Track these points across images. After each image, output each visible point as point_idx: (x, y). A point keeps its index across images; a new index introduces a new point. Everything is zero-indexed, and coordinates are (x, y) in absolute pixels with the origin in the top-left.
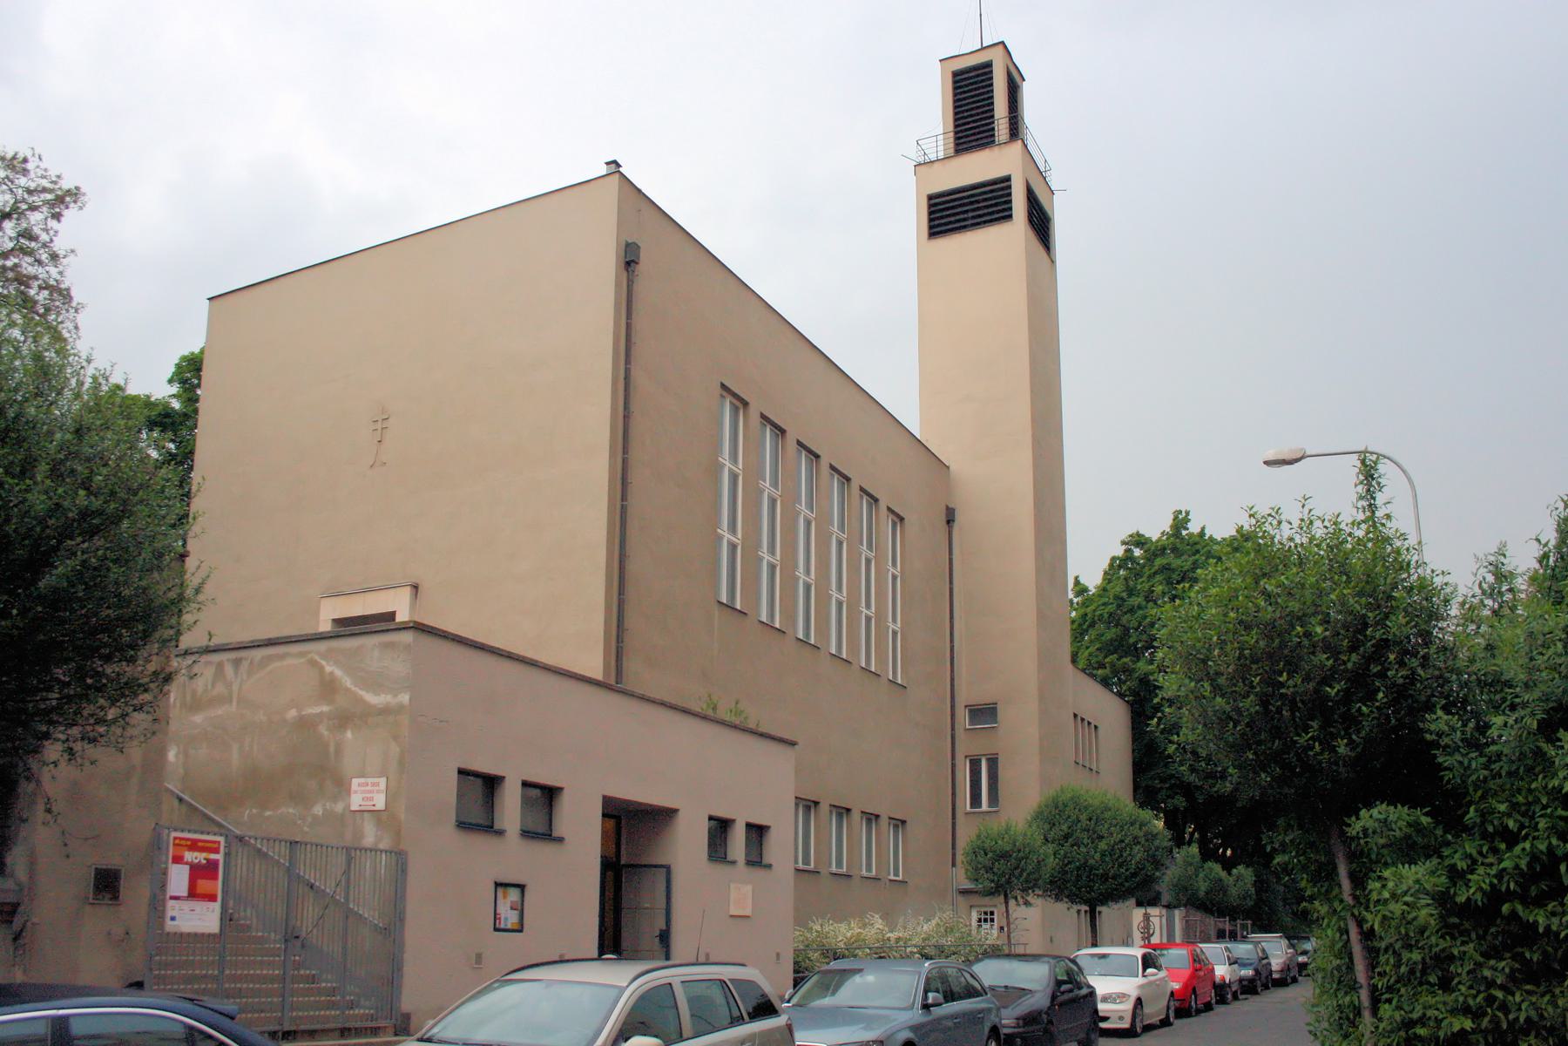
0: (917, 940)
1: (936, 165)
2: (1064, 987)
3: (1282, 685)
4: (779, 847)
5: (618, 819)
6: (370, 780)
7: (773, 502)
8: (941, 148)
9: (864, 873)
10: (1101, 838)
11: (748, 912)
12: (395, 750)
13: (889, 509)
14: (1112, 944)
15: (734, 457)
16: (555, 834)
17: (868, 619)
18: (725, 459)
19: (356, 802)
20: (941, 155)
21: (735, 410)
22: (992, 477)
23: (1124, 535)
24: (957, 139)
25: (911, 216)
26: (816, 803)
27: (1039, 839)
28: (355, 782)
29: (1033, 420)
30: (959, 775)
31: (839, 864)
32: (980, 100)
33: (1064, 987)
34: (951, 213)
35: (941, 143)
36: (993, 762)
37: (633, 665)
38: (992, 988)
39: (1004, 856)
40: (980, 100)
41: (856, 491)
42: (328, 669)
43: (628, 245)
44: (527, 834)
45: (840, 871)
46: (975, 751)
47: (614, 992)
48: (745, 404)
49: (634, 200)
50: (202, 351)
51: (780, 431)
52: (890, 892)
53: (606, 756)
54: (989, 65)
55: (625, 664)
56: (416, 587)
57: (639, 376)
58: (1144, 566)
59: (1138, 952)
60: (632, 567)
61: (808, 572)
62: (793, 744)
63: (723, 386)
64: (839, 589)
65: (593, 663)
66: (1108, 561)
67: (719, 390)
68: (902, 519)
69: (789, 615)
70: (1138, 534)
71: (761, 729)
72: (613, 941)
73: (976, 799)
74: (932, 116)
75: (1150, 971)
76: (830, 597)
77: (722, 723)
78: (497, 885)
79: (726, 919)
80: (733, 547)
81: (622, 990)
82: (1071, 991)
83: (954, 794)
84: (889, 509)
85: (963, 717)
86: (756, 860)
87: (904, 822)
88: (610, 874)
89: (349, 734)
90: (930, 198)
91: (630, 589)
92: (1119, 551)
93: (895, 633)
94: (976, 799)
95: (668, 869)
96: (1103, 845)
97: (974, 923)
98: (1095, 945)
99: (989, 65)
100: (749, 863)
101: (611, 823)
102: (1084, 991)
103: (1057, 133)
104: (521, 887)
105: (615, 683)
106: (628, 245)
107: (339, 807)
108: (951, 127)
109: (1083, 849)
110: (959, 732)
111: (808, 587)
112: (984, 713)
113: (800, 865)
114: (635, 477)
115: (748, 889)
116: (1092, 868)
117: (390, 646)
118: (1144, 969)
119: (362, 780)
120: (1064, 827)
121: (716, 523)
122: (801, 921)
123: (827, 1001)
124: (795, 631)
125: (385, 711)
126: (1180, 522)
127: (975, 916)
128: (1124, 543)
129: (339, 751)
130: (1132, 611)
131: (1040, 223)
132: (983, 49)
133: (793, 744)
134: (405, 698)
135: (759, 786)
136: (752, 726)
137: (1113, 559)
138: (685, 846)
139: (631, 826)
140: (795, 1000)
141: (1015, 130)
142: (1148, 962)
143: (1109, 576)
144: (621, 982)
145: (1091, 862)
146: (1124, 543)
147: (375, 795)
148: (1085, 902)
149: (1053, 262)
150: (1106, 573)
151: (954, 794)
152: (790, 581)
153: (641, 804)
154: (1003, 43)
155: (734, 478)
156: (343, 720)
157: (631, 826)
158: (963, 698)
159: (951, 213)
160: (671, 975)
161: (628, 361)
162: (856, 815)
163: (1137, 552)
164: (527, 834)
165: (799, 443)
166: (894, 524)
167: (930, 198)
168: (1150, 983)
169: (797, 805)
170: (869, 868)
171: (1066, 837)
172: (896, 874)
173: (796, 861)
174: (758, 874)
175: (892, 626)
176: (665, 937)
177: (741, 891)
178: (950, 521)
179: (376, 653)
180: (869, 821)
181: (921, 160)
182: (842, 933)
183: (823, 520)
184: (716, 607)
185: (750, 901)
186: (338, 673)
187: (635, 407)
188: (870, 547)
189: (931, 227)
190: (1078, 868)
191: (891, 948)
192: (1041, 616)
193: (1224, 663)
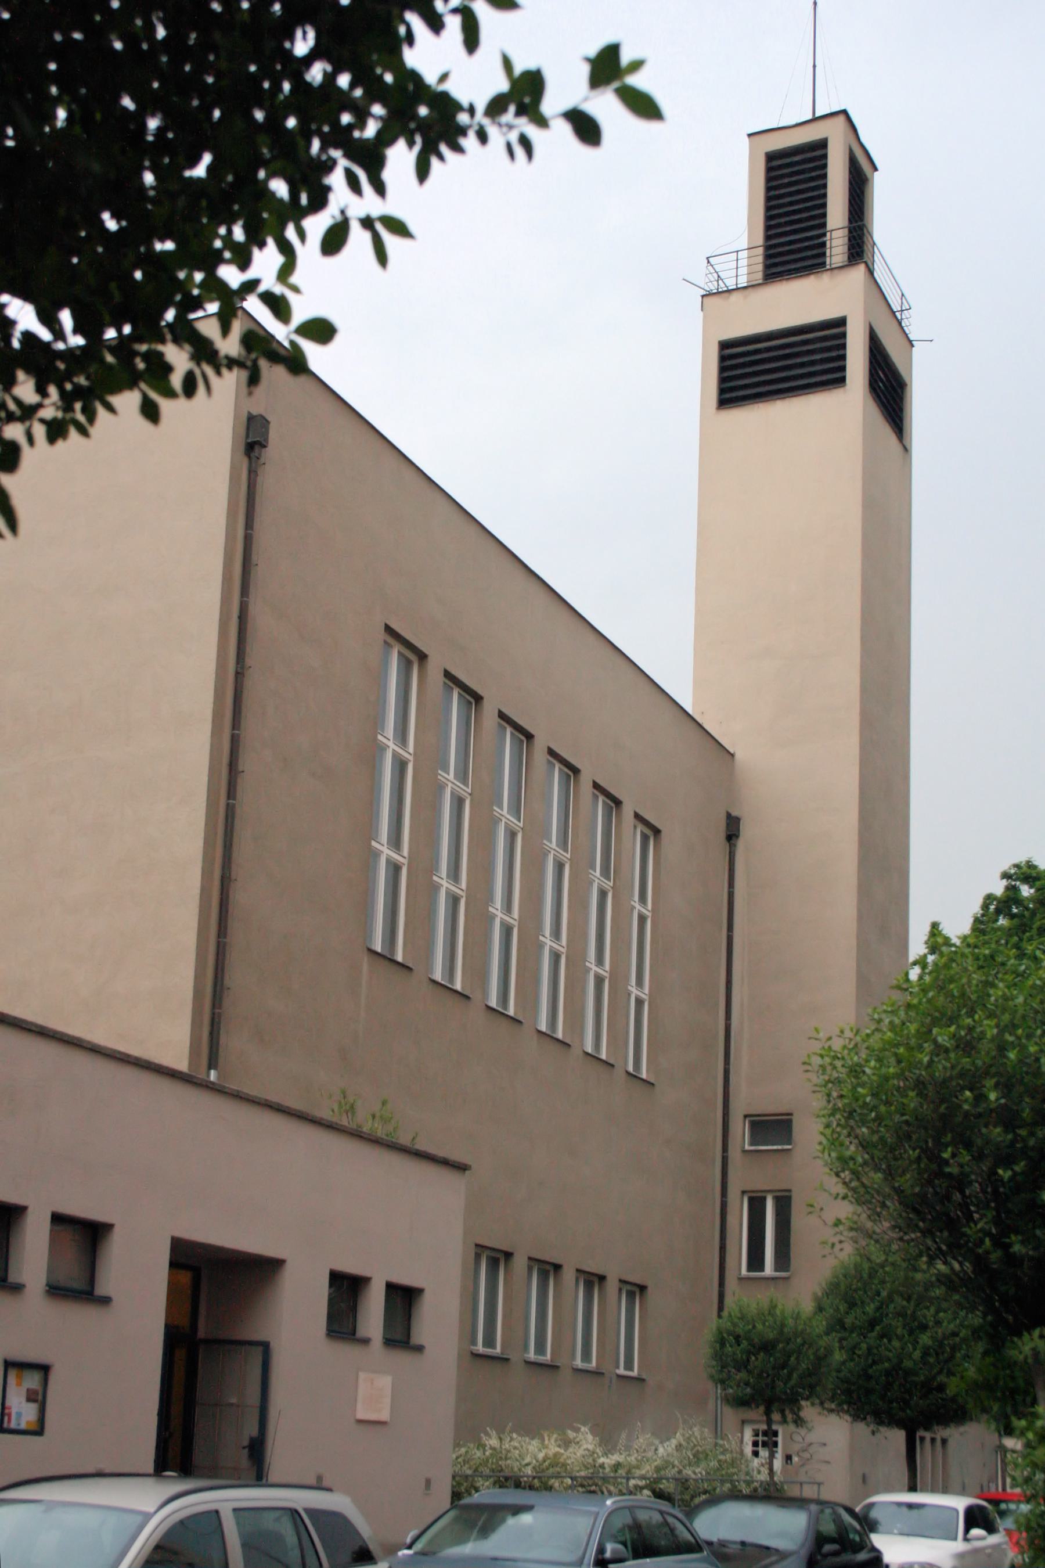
0: (647, 1469)
1: (735, 297)
2: (828, 1548)
3: (946, 1162)
4: (438, 1321)
5: (196, 1272)
7: (459, 802)
8: (743, 271)
9: (579, 1363)
10: (924, 1328)
11: (384, 1415)
13: (637, 816)
14: (933, 1490)
15: (402, 736)
16: (100, 1290)
17: (599, 981)
20: (743, 281)
21: (406, 665)
22: (797, 772)
23: (1006, 864)
24: (767, 257)
25: (695, 373)
26: (508, 1255)
27: (820, 1325)
29: (864, 690)
30: (731, 1220)
31: (540, 1348)
33: (828, 1548)
34: (755, 371)
35: (743, 263)
36: (784, 1204)
37: (236, 1042)
38: (710, 1544)
39: (767, 1347)
41: (586, 787)
43: (251, 419)
44: (56, 1291)
45: (541, 1359)
46: (759, 1182)
47: (139, 1519)
48: (422, 657)
52: (615, 1396)
53: (178, 1180)
54: (822, 145)
55: (223, 1039)
57: (258, 609)
58: (1034, 913)
59: (960, 1503)
60: (240, 897)
61: (508, 908)
62: (462, 1168)
63: (388, 629)
64: (556, 934)
65: (172, 1042)
66: (979, 901)
67: (381, 635)
68: (657, 832)
69: (478, 972)
70: (1030, 865)
71: (422, 1146)
72: (178, 1451)
73: (756, 1261)
74: (731, 218)
75: (976, 1532)
76: (541, 946)
77: (357, 1135)
78: (8, 1364)
79: (349, 1429)
80: (395, 869)
81: (148, 1517)
82: (836, 1554)
83: (723, 1248)
84: (637, 816)
85: (741, 1132)
86: (400, 1337)
87: (642, 1288)
88: (180, 1354)
90: (724, 345)
91: (235, 927)
92: (998, 888)
93: (639, 1002)
94: (756, 1261)
95: (266, 1347)
96: (925, 1339)
97: (748, 1449)
98: (913, 1488)
99: (822, 145)
100: (390, 1342)
101: (185, 1278)
102: (862, 1556)
103: (924, 257)
104: (44, 1369)
105: (209, 1069)
106: (251, 419)
108: (760, 240)
109: (896, 1343)
110: (734, 1154)
111: (507, 931)
112: (773, 1128)
113: (480, 1348)
114: (248, 763)
115: (385, 1382)
116: (908, 1373)
118: (967, 1530)
120: (870, 1308)
121: (370, 831)
122: (467, 1430)
123: (469, 1548)
124: (485, 993)
127: (748, 1436)
128: (1005, 876)
131: (889, 391)
132: (815, 119)
133: (462, 1168)
135: (408, 1228)
136: (404, 1140)
137: (989, 898)
138: (294, 1315)
139: (215, 1286)
140: (419, 1546)
141: (859, 247)
142: (974, 1518)
143: (981, 925)
144: (153, 1506)
145: (908, 1364)
146: (1005, 876)
148: (900, 1424)
149: (906, 450)
150: (977, 920)
151: (723, 1248)
152: (481, 920)
153: (221, 1249)
154: (844, 112)
155: (401, 766)
157: (215, 1286)
158: (740, 1107)
159: (755, 371)
160: (226, 1499)
161: (245, 590)
163: (1026, 891)
164: (56, 1291)
166: (645, 838)
167: (724, 345)
168: (976, 1551)
169: (478, 1257)
170: (586, 1355)
171: (872, 1323)
172: (629, 1366)
173: (474, 1342)
174: (402, 1359)
175: (634, 991)
176: (257, 1450)
177: (374, 1384)
180: (589, 1286)
181: (713, 287)
182: (530, 1452)
183: (537, 831)
184: (365, 962)
185: (387, 1401)
187: (237, 871)
188: (605, 872)
189: (722, 391)
190: (888, 1373)
191: (605, 1479)
192: (863, 982)
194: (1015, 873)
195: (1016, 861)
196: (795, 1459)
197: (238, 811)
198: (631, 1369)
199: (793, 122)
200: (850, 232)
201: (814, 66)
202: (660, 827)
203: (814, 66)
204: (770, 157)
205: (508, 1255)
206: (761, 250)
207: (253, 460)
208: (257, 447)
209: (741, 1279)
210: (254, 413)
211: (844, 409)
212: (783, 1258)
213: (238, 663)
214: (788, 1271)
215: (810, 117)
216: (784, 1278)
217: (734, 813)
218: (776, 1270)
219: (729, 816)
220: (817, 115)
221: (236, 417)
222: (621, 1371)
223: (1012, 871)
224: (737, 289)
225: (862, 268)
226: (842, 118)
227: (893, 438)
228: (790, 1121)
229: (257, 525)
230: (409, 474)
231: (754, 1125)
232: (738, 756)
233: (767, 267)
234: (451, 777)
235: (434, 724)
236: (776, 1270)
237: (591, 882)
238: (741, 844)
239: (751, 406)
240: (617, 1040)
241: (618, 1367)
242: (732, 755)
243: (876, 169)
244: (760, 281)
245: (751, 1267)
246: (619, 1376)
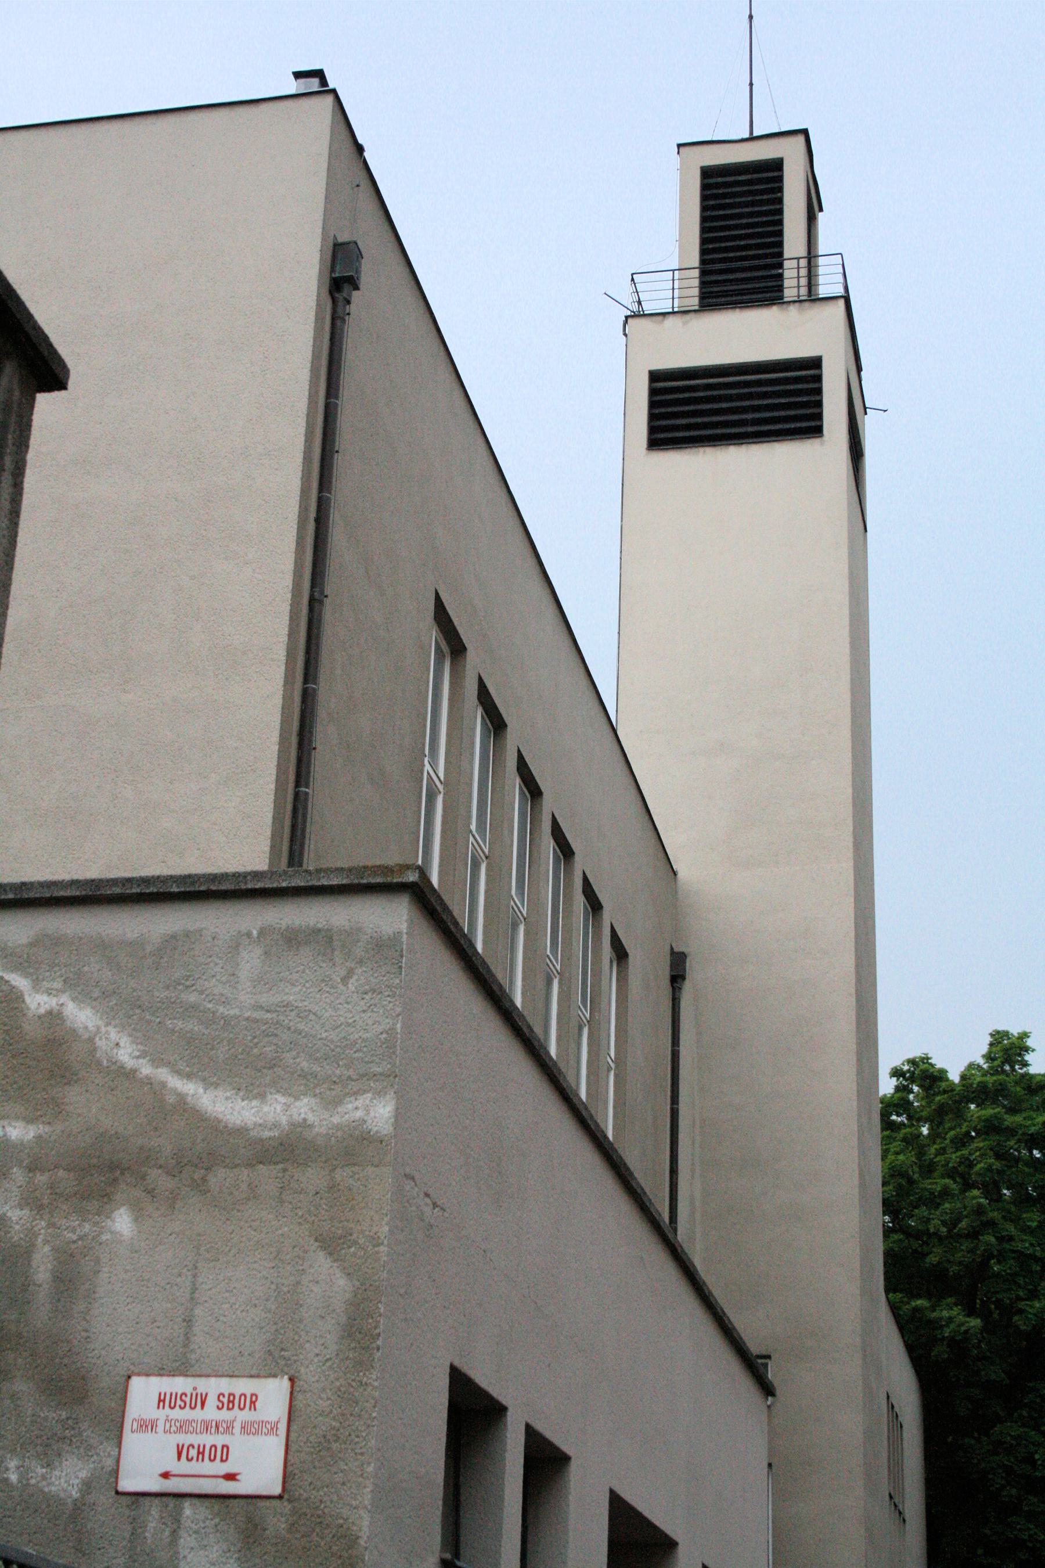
1: (670, 321)
6: (213, 1387)
12: (328, 1283)
19: (145, 1460)
28: (143, 1394)
32: (745, 223)
40: (745, 223)
42: (38, 1002)
54: (776, 166)
74: (666, 236)
89: (122, 1222)
90: (655, 377)
99: (776, 166)
107: (67, 1478)
108: (695, 260)
117: (324, 940)
119: (180, 1385)
125: (287, 1150)
126: (1008, 1050)
129: (71, 1279)
130: (933, 1201)
132: (752, 139)
134: (379, 1113)
147: (237, 1442)
156: (99, 1174)
159: (689, 411)
167: (655, 377)
178: (677, 978)
179: (250, 960)
186: (81, 1016)
189: (652, 430)
194: (909, 1071)
195: (911, 1056)
199: (739, 137)
201: (751, 84)
203: (751, 84)
204: (707, 173)
206: (696, 273)
207: (340, 304)
208: (346, 288)
210: (340, 240)
213: (313, 586)
215: (747, 135)
220: (755, 134)
221: (324, 240)
223: (906, 1068)
224: (673, 313)
226: (801, 139)
230: (458, 393)
238: (687, 987)
239: (695, 450)
242: (675, 873)
243: (821, 209)
244: (697, 308)
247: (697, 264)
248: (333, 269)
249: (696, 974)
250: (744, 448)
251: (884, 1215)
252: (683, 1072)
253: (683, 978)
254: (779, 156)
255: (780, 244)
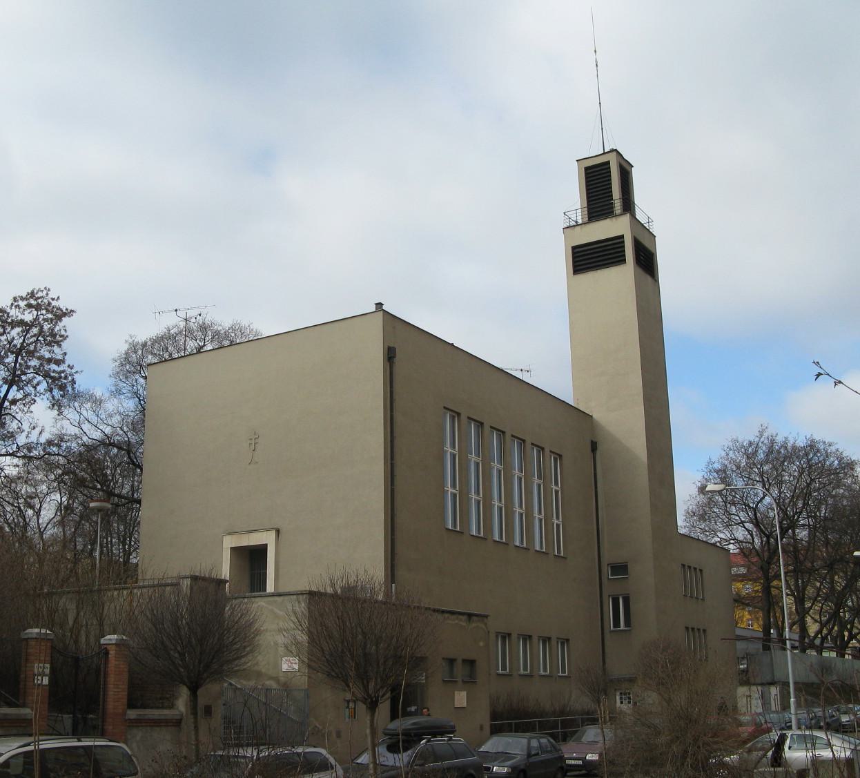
9: (542, 673)
18: (448, 448)
20: (580, 221)
22: (623, 422)
25: (561, 261)
32: (605, 185)
34: (587, 258)
37: (401, 573)
40: (605, 185)
43: (389, 348)
49: (393, 323)
50: (138, 424)
51: (480, 424)
54: (608, 163)
56: (278, 531)
64: (521, 506)
68: (560, 456)
69: (488, 528)
73: (617, 624)
85: (607, 572)
87: (568, 640)
90: (574, 248)
94: (617, 624)
99: (608, 163)
102: (186, 583)
103: (653, 201)
106: (389, 348)
110: (605, 581)
112: (620, 569)
115: (464, 694)
124: (492, 536)
131: (646, 261)
132: (604, 153)
141: (628, 205)
154: (616, 150)
158: (605, 562)
159: (587, 258)
162: (535, 639)
165: (491, 427)
167: (574, 248)
170: (545, 670)
172: (564, 671)
174: (687, 626)
175: (555, 521)
183: (508, 469)
187: (396, 434)
188: (539, 477)
193: (311, 775)
196: (638, 704)
197: (395, 490)
198: (565, 672)
200: (623, 200)
202: (561, 454)
204: (587, 169)
205: (509, 635)
206: (586, 209)
209: (611, 632)
211: (623, 276)
212: (628, 623)
214: (630, 627)
216: (629, 630)
217: (594, 440)
218: (626, 627)
219: (592, 441)
222: (560, 674)
225: (628, 215)
227: (649, 278)
228: (627, 566)
229: (396, 483)
231: (612, 568)
232: (594, 416)
233: (589, 213)
234: (473, 456)
235: (464, 438)
236: (626, 627)
237: (534, 482)
238: (598, 453)
240: (549, 543)
241: (559, 672)
242: (591, 416)
245: (614, 627)
246: (559, 676)
247: (586, 206)
248: (388, 355)
249: (600, 448)
250: (599, 271)
251: (137, 565)
252: (598, 477)
253: (596, 449)
254: (265, 543)
255: (612, 196)
